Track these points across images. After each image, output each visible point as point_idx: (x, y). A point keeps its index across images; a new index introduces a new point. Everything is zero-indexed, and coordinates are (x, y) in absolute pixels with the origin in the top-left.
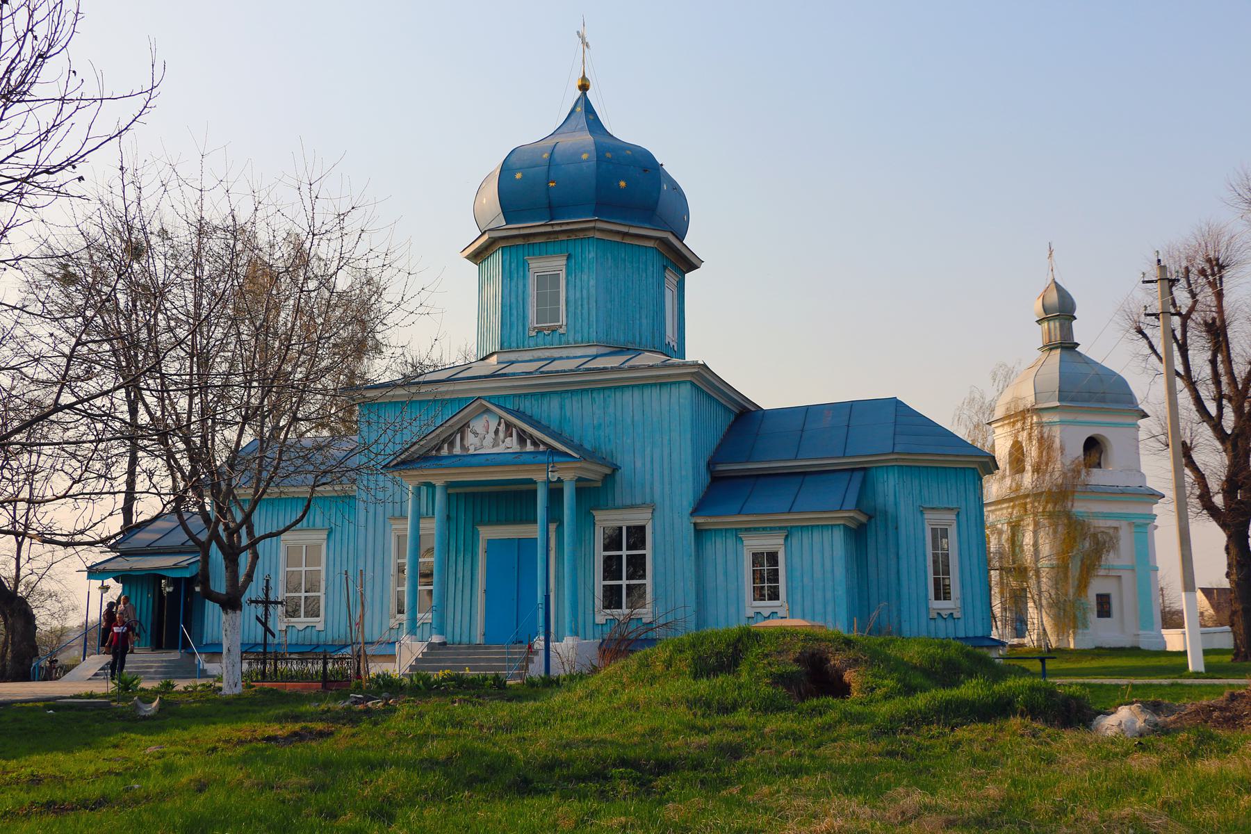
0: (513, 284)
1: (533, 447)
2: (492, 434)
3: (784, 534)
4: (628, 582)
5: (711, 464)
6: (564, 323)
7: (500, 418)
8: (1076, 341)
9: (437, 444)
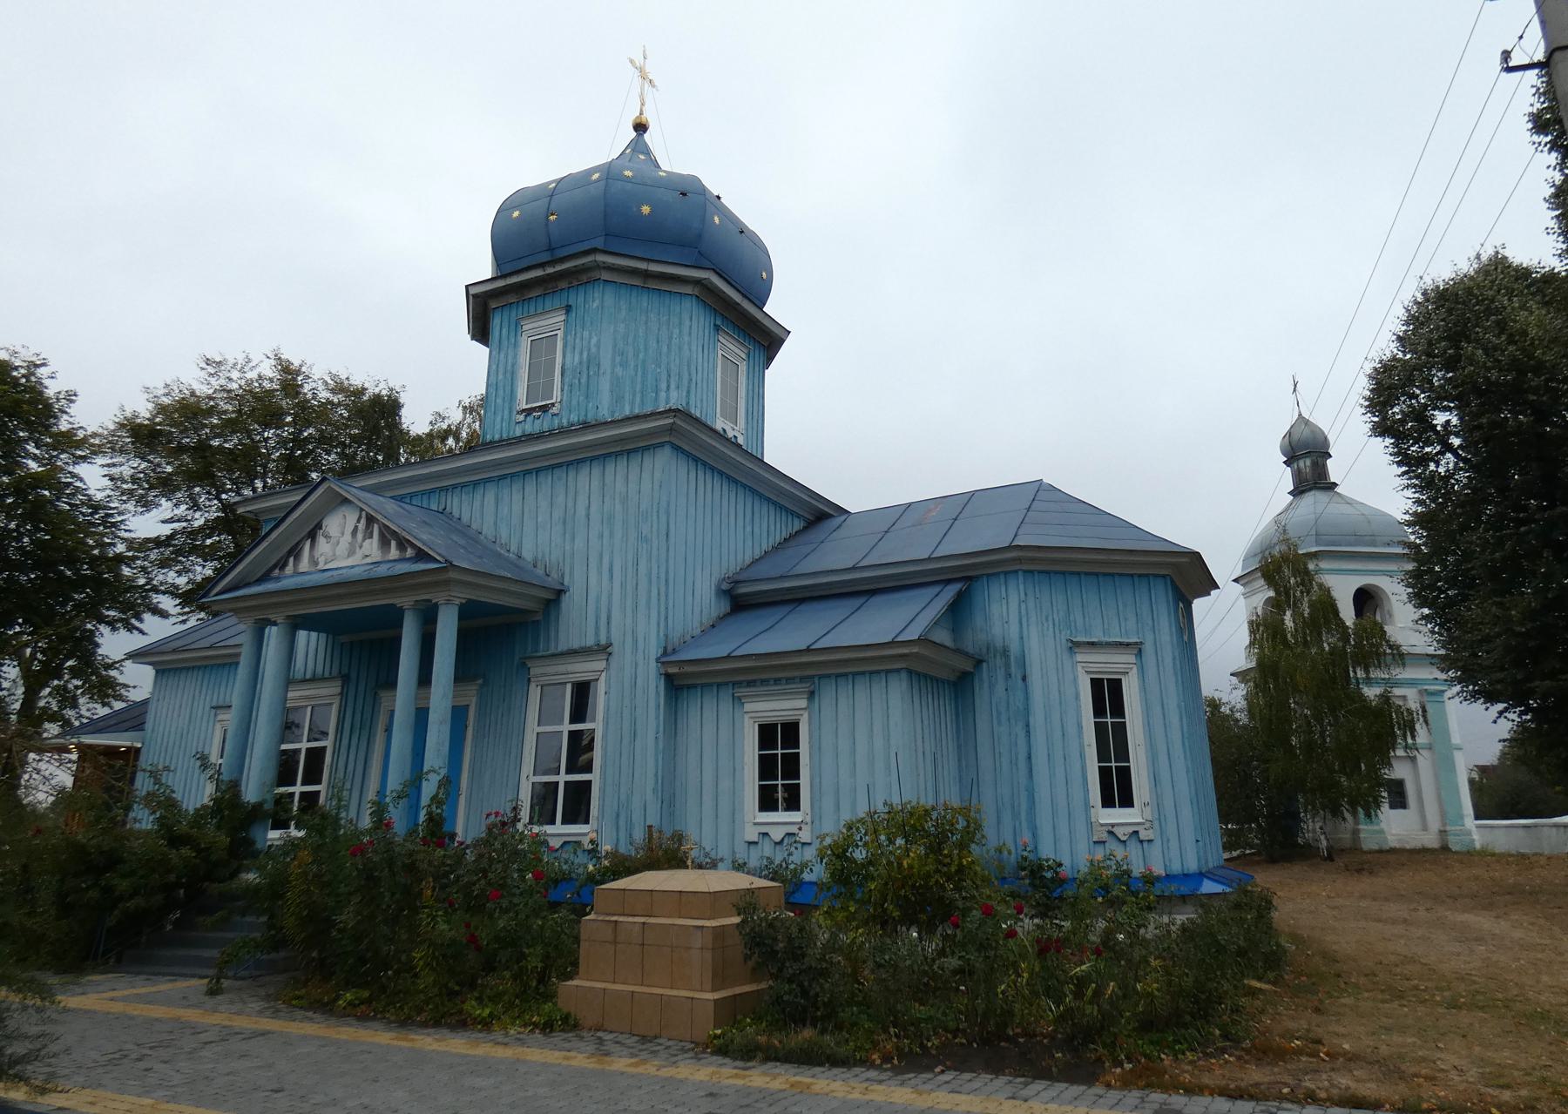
0: (502, 356)
2: (348, 537)
3: (805, 687)
4: (291, 789)
7: (362, 510)
8: (1332, 480)
9: (282, 558)
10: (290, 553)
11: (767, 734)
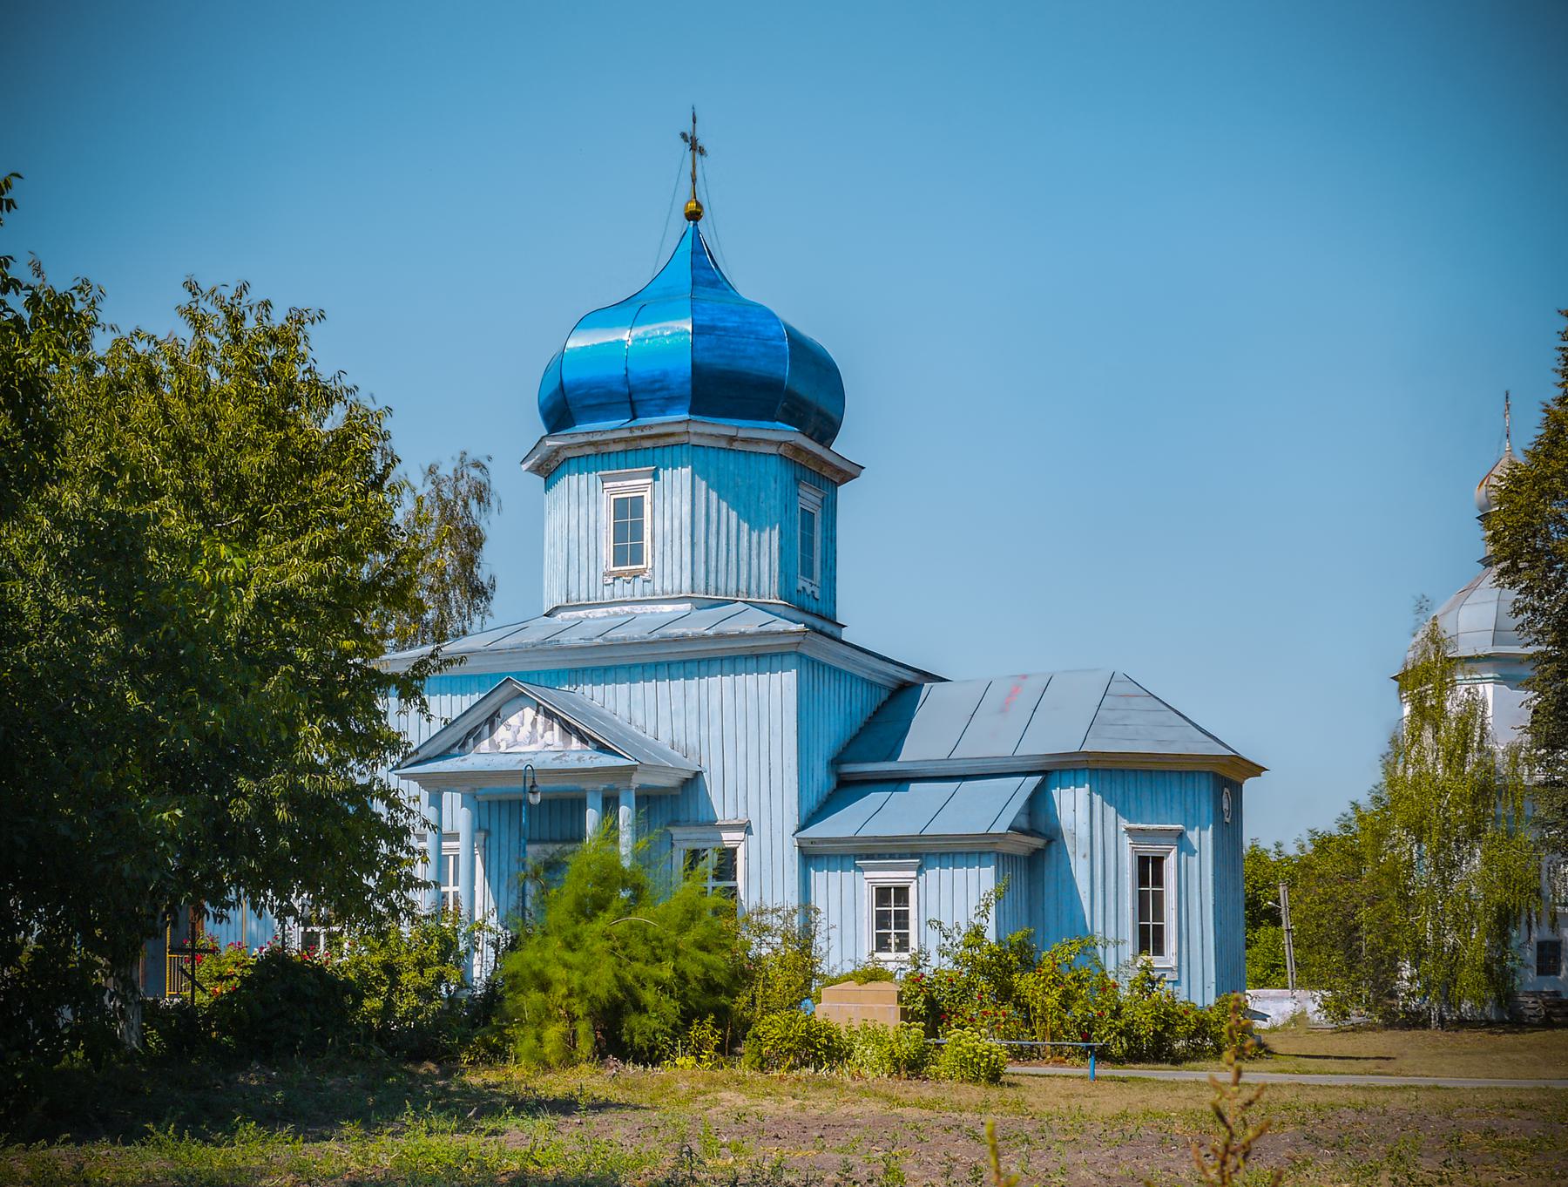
1: (579, 744)
5: (836, 762)
6: (650, 566)
7: (539, 704)
10: (469, 735)
11: (882, 894)
